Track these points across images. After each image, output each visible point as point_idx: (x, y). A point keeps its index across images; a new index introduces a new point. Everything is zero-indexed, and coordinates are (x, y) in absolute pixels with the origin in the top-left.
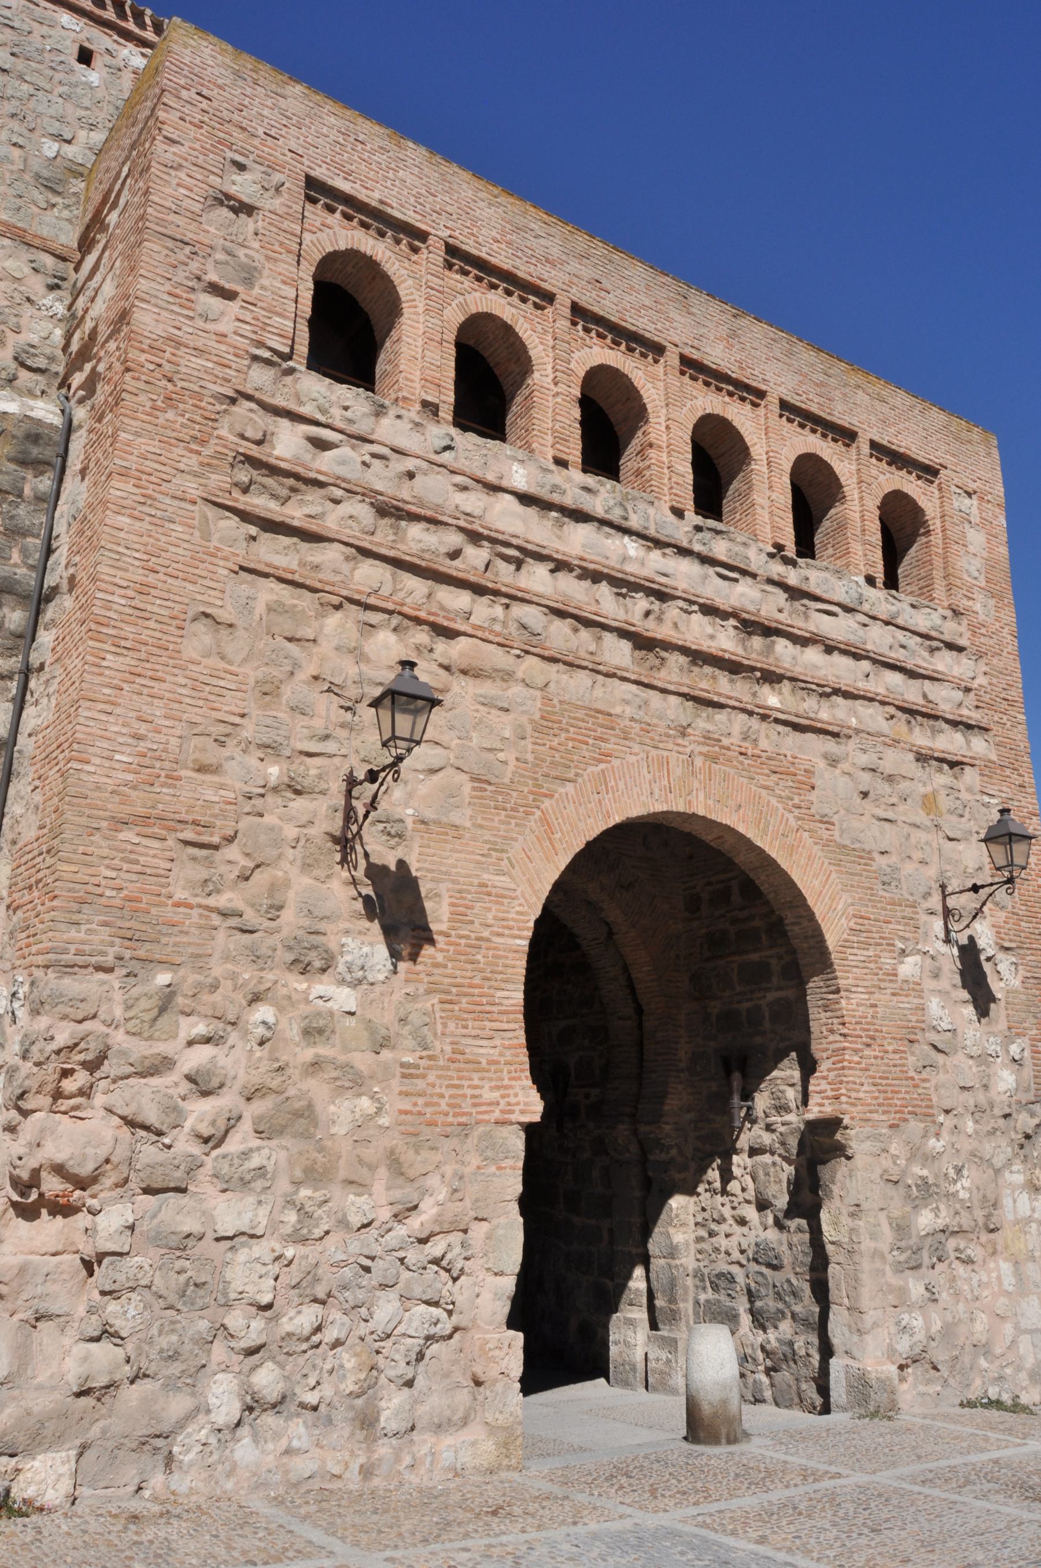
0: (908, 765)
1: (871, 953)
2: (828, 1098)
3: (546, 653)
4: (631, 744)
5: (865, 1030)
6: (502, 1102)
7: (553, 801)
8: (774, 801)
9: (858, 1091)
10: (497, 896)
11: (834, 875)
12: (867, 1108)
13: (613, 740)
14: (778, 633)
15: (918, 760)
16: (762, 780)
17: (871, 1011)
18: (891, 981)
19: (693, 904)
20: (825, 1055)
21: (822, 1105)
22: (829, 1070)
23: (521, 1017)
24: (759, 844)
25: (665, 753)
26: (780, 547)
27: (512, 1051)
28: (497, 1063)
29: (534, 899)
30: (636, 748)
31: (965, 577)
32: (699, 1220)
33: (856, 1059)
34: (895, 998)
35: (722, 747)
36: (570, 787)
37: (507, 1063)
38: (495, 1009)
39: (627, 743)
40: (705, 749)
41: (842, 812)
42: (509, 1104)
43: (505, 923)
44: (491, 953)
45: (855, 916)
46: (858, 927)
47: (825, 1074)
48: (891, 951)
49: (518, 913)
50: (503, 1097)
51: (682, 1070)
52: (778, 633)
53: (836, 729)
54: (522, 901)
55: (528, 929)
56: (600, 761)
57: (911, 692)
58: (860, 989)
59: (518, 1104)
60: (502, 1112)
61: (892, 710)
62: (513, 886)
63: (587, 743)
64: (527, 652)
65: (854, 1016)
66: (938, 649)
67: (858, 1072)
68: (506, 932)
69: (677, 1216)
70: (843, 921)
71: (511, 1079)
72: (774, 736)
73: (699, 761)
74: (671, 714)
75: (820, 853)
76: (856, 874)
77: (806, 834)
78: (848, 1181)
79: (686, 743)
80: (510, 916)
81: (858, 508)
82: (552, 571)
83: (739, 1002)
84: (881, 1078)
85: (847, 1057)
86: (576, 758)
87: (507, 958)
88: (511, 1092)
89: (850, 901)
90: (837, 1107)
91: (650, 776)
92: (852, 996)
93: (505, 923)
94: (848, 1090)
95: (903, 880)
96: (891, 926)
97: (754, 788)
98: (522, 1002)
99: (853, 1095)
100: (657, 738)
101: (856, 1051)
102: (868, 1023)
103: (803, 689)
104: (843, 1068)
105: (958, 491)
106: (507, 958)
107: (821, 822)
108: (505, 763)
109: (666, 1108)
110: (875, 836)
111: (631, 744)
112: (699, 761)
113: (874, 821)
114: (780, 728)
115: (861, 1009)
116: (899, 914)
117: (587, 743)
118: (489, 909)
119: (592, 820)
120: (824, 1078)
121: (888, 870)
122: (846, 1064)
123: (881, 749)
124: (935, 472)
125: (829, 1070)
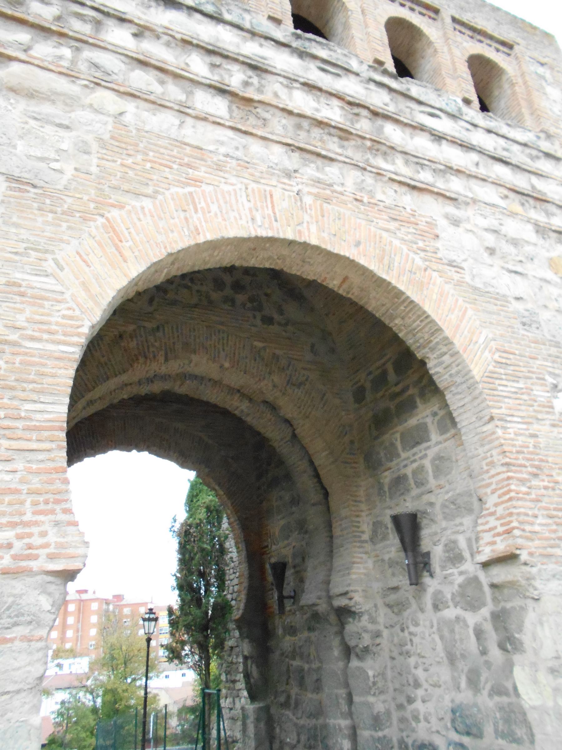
0: (527, 233)
1: (521, 385)
2: (499, 534)
3: (122, 89)
4: (226, 175)
5: (528, 460)
6: (18, 545)
7: (123, 212)
8: (396, 243)
9: (532, 524)
10: (33, 297)
11: (470, 312)
12: (545, 543)
13: (203, 169)
14: (386, 117)
15: (537, 232)
16: (382, 224)
17: (532, 441)
18: (548, 413)
19: (359, 395)
20: (489, 490)
21: (494, 543)
22: (496, 505)
23: (63, 435)
24: (384, 276)
25: (268, 188)
26: (380, 63)
27: (44, 477)
28: (17, 491)
29: (91, 304)
30: (233, 180)
31: (550, 112)
32: (397, 686)
33: (524, 489)
34: (556, 430)
35: (333, 191)
36: (147, 203)
37: (30, 492)
38: (19, 424)
39: (221, 174)
40: (315, 190)
41: (471, 261)
42: (30, 547)
43: (45, 327)
44: (18, 359)
45: (498, 350)
46: (504, 361)
47: (492, 510)
48: (542, 385)
49: (64, 317)
50: (19, 537)
51: (366, 542)
52: (386, 117)
53: (453, 196)
54: (72, 304)
55: (79, 335)
56: (188, 185)
57: (522, 182)
58: (515, 419)
59: (46, 546)
60: (15, 557)
61: (506, 192)
62: (59, 288)
63: (171, 168)
64: (98, 84)
65: (514, 446)
66: (538, 157)
67: (529, 504)
68: (45, 336)
69: (374, 683)
70: (487, 353)
71: (34, 513)
72: (391, 192)
73: (308, 200)
74: (274, 159)
75: (452, 291)
76: (493, 313)
77: (435, 274)
78: (539, 628)
79: (294, 184)
80: (53, 319)
81: (448, 57)
82: (135, 35)
83: (405, 466)
84: (555, 509)
85: (513, 487)
86: (155, 177)
87: (44, 365)
88: (35, 530)
89: (491, 336)
90: (510, 541)
91: (251, 205)
92: (509, 425)
93: (45, 327)
94: (521, 523)
95: (543, 323)
96: (538, 362)
97: (373, 229)
98: (64, 417)
99: (528, 528)
100: (257, 174)
101: (522, 481)
102: (530, 453)
103: (417, 163)
104: (510, 499)
105: (531, 60)
106: (44, 365)
107: (448, 265)
108: (61, 172)
109: (354, 577)
110: (506, 284)
111: (226, 175)
112: (308, 200)
113: (505, 272)
114: (396, 186)
115: (520, 438)
116: (544, 352)
117: (171, 168)
118: (22, 311)
119: (175, 234)
120: (492, 514)
121: (526, 314)
122: (513, 494)
123: (500, 217)
124: (511, 47)
125: (496, 505)
